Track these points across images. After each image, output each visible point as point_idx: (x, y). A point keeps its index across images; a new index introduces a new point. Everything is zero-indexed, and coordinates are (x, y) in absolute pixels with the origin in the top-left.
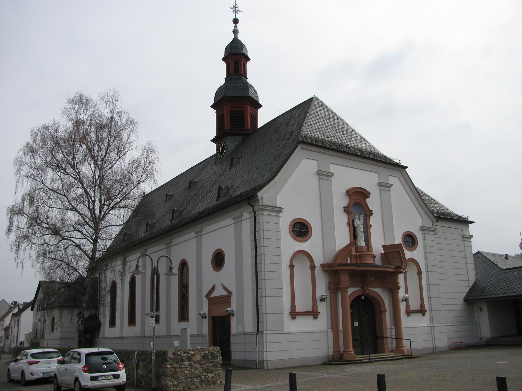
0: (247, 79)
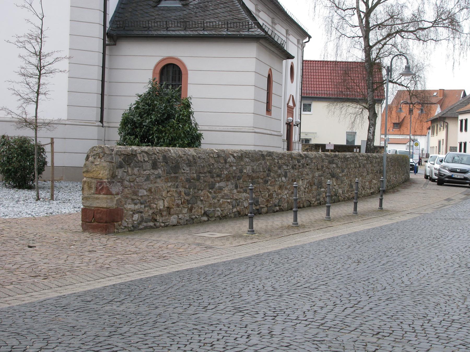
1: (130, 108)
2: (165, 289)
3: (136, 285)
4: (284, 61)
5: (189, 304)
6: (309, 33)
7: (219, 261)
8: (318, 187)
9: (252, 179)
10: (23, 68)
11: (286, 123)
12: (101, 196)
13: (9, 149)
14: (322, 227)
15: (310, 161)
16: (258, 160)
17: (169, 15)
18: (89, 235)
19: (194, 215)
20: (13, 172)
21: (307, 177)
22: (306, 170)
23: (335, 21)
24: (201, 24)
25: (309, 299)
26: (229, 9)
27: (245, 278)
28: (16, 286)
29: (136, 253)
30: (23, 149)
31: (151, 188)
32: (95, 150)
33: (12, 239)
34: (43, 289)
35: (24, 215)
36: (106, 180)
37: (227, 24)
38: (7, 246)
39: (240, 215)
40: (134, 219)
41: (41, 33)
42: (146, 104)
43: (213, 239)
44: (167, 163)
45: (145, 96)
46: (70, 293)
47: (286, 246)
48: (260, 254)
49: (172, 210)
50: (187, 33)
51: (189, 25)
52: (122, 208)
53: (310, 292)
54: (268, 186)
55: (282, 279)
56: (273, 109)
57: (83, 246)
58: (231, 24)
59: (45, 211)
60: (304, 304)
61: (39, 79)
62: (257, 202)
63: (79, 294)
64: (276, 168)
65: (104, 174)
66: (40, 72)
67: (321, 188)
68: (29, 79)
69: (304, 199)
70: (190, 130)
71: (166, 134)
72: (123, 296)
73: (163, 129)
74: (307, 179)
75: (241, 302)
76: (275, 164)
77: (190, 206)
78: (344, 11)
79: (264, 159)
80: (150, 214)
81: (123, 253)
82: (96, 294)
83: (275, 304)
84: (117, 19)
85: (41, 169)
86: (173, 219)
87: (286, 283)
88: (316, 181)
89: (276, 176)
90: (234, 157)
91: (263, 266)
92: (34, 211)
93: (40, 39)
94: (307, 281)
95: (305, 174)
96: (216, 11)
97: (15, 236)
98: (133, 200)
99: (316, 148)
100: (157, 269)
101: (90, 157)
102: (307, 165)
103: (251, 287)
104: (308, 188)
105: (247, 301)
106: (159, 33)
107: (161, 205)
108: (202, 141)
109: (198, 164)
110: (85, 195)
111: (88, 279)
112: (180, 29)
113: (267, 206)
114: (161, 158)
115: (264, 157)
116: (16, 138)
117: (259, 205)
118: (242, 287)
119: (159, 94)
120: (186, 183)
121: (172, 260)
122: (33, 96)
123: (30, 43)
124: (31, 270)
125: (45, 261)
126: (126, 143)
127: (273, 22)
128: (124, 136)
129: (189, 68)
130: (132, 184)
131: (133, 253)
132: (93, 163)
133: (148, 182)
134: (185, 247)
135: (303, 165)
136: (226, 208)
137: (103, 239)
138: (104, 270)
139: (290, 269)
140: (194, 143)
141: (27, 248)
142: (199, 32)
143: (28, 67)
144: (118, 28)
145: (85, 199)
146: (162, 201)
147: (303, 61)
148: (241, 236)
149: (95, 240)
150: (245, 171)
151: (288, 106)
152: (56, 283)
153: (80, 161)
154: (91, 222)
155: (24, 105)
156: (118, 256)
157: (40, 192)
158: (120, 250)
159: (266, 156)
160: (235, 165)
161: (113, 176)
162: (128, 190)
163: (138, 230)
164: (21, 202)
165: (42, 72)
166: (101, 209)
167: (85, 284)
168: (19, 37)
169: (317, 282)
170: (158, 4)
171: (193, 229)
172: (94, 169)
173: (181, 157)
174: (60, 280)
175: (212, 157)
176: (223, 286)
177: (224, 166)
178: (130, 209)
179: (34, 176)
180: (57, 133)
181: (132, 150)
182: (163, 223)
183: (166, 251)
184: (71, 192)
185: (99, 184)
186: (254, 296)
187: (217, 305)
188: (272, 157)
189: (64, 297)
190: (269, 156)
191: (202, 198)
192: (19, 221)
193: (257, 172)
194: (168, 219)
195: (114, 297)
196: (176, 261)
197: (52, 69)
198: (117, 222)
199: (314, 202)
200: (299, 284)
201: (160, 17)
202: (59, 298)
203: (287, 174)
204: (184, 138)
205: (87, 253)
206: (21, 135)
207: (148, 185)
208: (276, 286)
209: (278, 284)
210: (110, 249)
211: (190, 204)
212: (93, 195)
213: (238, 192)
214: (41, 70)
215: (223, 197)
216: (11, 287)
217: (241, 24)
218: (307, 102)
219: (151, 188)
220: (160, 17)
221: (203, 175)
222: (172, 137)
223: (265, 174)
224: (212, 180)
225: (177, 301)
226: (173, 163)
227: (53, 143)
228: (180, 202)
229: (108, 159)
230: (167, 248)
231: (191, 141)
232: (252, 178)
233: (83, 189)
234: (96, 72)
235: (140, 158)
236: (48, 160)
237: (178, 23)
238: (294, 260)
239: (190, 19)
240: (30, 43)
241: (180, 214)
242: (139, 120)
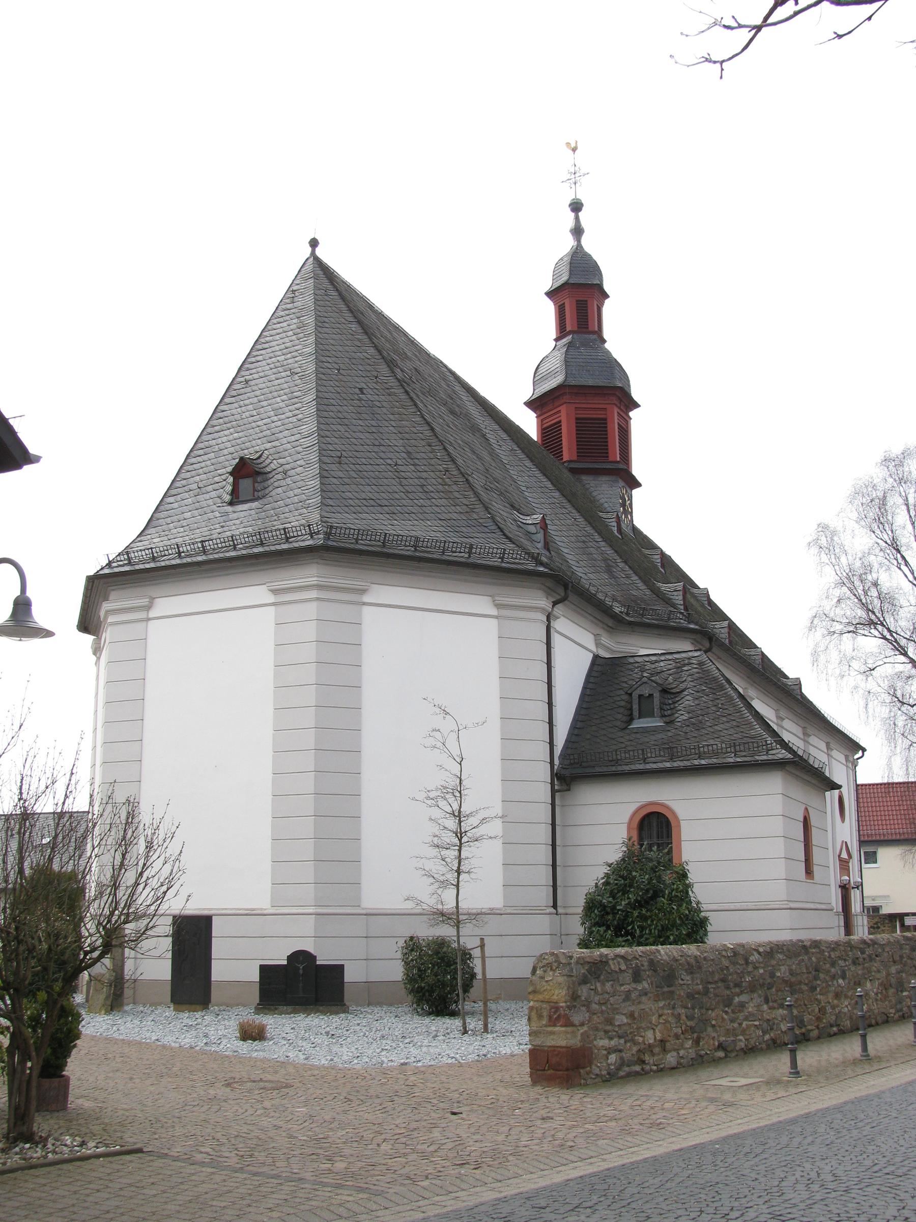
0: (604, 341)
1: (596, 884)
2: (661, 1183)
3: (615, 1177)
4: (828, 794)
5: (699, 1209)
6: (862, 744)
7: (746, 1128)
8: (897, 990)
9: (791, 986)
10: (437, 836)
11: (840, 886)
12: (557, 1029)
13: (421, 957)
14: (908, 1058)
15: (880, 950)
16: (797, 955)
17: (646, 740)
19: (703, 1050)
20: (428, 991)
21: (878, 976)
22: (876, 965)
23: (900, 723)
24: (695, 749)
25: (894, 1196)
26: (734, 723)
27: (788, 1158)
28: (433, 1182)
29: (613, 1119)
30: (440, 955)
32: (544, 959)
33: (428, 1100)
34: (474, 1187)
35: (445, 1059)
36: (564, 1004)
37: (735, 746)
38: (419, 1113)
39: (775, 1045)
41: (460, 783)
42: (620, 877)
43: (734, 1090)
44: (655, 971)
45: (617, 864)
46: (513, 1192)
47: (852, 1096)
48: (810, 1113)
49: (668, 1044)
50: (675, 764)
51: (677, 752)
53: (895, 1181)
54: (817, 994)
55: (848, 1158)
56: (816, 869)
57: (533, 1110)
58: (739, 745)
59: (476, 1051)
60: (886, 1204)
61: (460, 851)
62: (802, 1021)
63: (527, 1195)
64: (828, 965)
65: (559, 995)
66: (460, 840)
67: (902, 991)
68: (444, 853)
69: (876, 1011)
70: (689, 912)
71: (652, 921)
72: (595, 1198)
73: (649, 914)
74: (878, 979)
75: (782, 1205)
76: (825, 959)
77: (695, 1035)
78: (912, 706)
79: (807, 953)
81: (595, 1119)
82: (554, 1193)
83: (838, 1206)
84: (570, 751)
85: (468, 986)
86: (671, 1059)
87: (855, 1165)
88: (893, 981)
89: (828, 978)
90: (759, 953)
91: (816, 1136)
92: (459, 1052)
93: (459, 791)
94: (889, 1161)
95: (875, 972)
96: (716, 727)
97: (432, 1096)
98: (606, 1032)
99: (891, 921)
100: (649, 1146)
102: (877, 956)
103: (798, 1174)
104: (881, 993)
105: (793, 1201)
106: (633, 767)
107: (650, 1037)
108: (709, 928)
109: (704, 970)
111: (542, 1167)
112: (664, 759)
113: (817, 1027)
114: (646, 964)
115: (807, 949)
116: (430, 938)
117: (806, 1026)
118: (783, 1176)
119: (639, 860)
120: (688, 1000)
121: (670, 1129)
122: (452, 877)
123: (446, 799)
124: (455, 1154)
125: (476, 1137)
126: (593, 938)
127: (805, 734)
128: (590, 928)
129: (681, 816)
130: (604, 1008)
131: (610, 1120)
132: (542, 978)
133: (628, 1003)
134: (692, 1105)
135: (870, 956)
136: (753, 1035)
137: (563, 1097)
138: (566, 1150)
139: (860, 1139)
140: (697, 932)
141: (449, 1115)
142: (692, 761)
143: (443, 835)
144: (571, 764)
146: (652, 1031)
147: (857, 786)
148: (779, 1082)
149: (551, 1100)
150: (778, 974)
151: (841, 860)
152: (493, 1174)
153: (523, 969)
154: (544, 1070)
155: (439, 891)
156: (587, 1126)
157: (468, 1020)
158: (590, 1115)
159: (810, 948)
160: (762, 965)
161: (574, 997)
162: (598, 1017)
163: (618, 1078)
164: (439, 1038)
165: (463, 841)
167: (536, 1176)
168: (428, 791)
169: (906, 1162)
170: (629, 725)
171: (703, 1074)
172: (545, 988)
173: (677, 960)
174: (499, 1171)
175: (724, 957)
176: (754, 1175)
177: (744, 969)
178: (602, 1046)
179: (458, 995)
180: (492, 926)
181: (601, 955)
182: (655, 1065)
183: (661, 1114)
184: (513, 1019)
185: (553, 1010)
186: (804, 1192)
187: (744, 1211)
188: (819, 948)
189: (505, 1200)
190: (814, 948)
191: (713, 1022)
192: (437, 1069)
193: (797, 974)
194: (662, 1059)
195: (582, 1200)
196: (678, 1132)
197: (478, 835)
198: (583, 1068)
199: (892, 1015)
200: (876, 1168)
201: (633, 743)
202: (497, 1202)
203: (845, 974)
204: (681, 925)
205: (539, 1122)
206: (437, 935)
207: (628, 1008)
208: (839, 1172)
209: (841, 1168)
210: (574, 1114)
211: (695, 1032)
212: (545, 1028)
213: (770, 1009)
214: (462, 837)
215: (746, 1019)
216: (425, 1183)
218: (870, 849)
220: (633, 743)
221: (713, 986)
222: (662, 925)
223: (810, 975)
224: (728, 992)
225: (680, 1206)
226: (664, 971)
227: (484, 945)
229: (565, 972)
230: (663, 1109)
231: (693, 930)
232: (791, 985)
233: (529, 1019)
234: (543, 833)
235: (613, 966)
236: (478, 970)
237: (660, 750)
238: (867, 1121)
239: (678, 743)
240: (446, 799)
241: (680, 1050)
242: (611, 902)
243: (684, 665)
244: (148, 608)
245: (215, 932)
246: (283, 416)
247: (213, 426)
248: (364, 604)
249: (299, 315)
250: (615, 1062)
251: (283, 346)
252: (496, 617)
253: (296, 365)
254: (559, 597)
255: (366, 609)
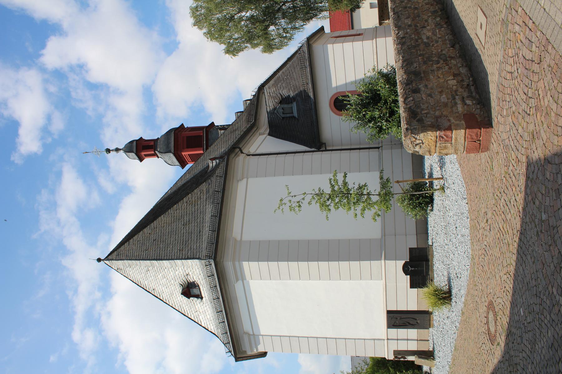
18: (495, 145)
31: (438, 91)
40: (471, 104)
49: (455, 72)
52: (462, 115)
54: (419, 7)
62: (434, 11)
77: (448, 59)
80: (463, 90)
101: (415, 150)
110: (453, 152)
145: (457, 151)
154: (480, 144)
160: (405, 31)
166: (466, 135)
172: (427, 145)
178: (462, 108)
185: (441, 139)
191: (440, 50)
194: (465, 75)
215: (436, 35)
217: (302, 58)
219: (438, 91)
221: (419, 52)
228: (447, 67)
243: (270, 95)
244: (249, 335)
245: (394, 309)
246: (165, 275)
247: (172, 304)
248: (241, 239)
249: (126, 267)
250: (472, 101)
251: (139, 274)
252: (248, 179)
253: (145, 268)
254: (240, 152)
255: (244, 239)
